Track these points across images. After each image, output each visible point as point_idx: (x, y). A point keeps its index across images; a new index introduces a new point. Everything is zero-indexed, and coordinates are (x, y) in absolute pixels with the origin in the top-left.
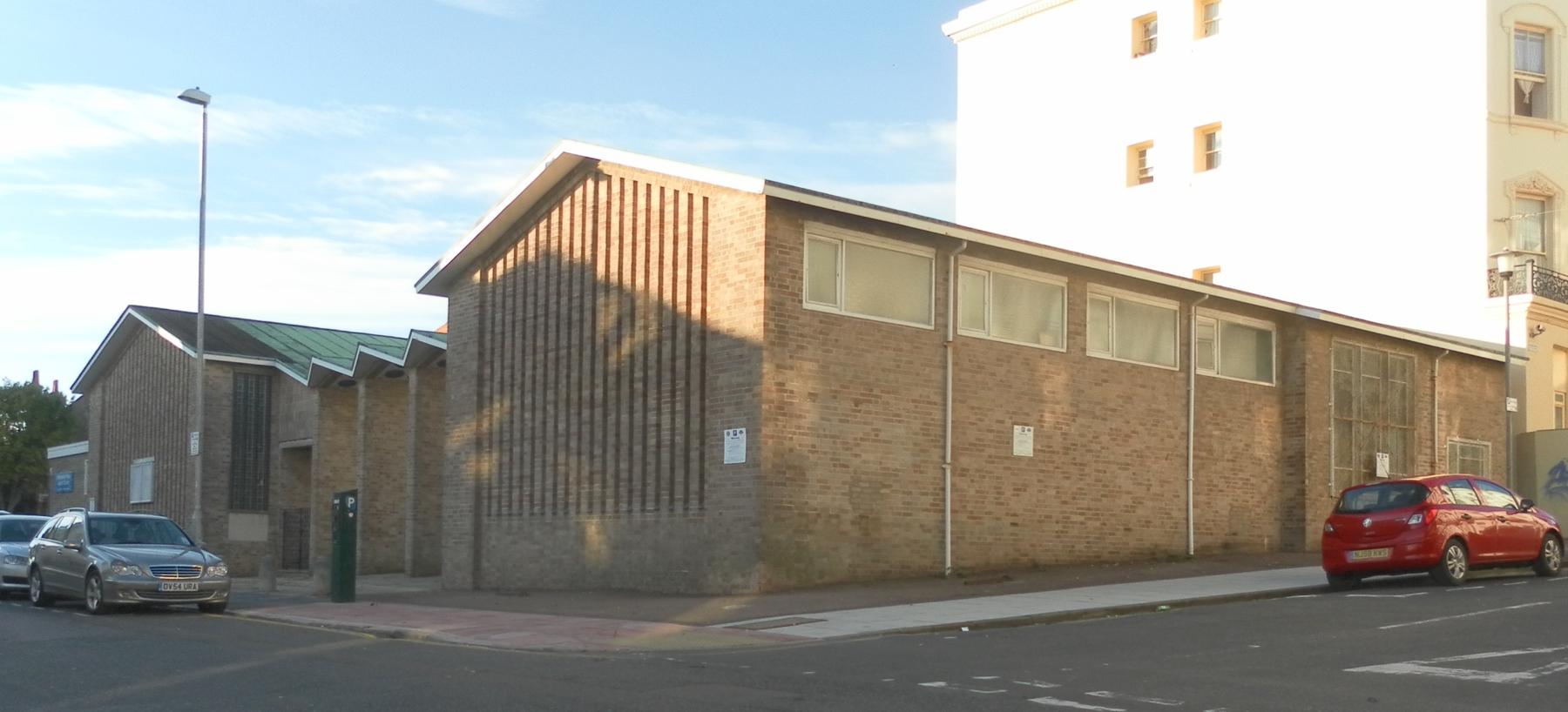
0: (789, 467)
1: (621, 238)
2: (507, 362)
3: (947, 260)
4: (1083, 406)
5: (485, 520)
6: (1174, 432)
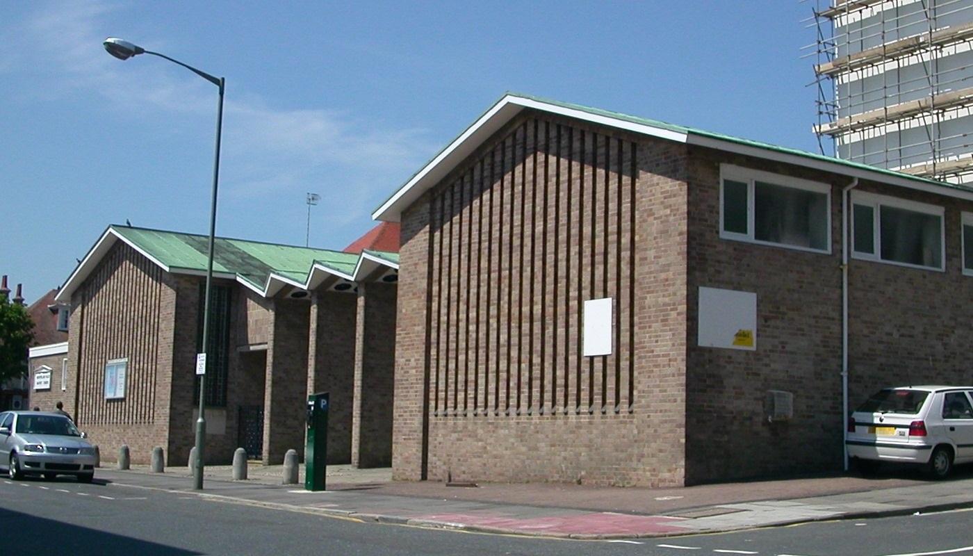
5: (432, 418)
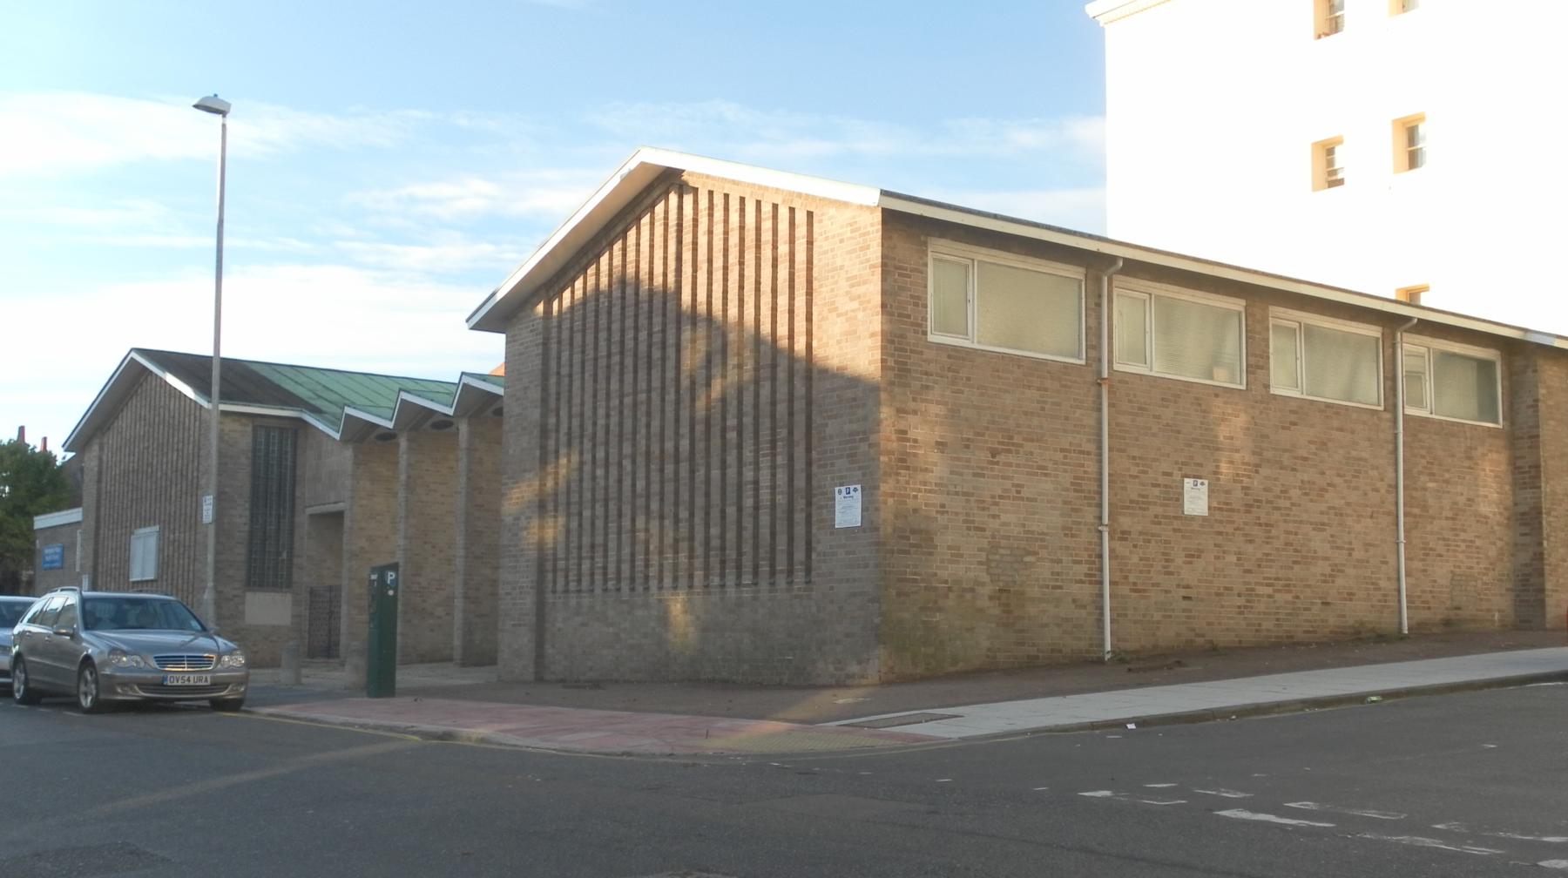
1: (710, 261)
3: (1099, 281)
4: (1268, 454)
6: (1379, 484)
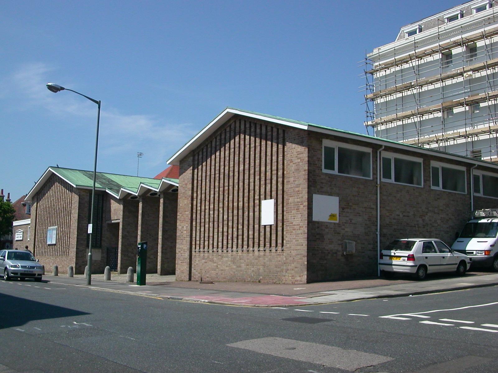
0: (318, 234)
2: (203, 192)
5: (193, 253)
